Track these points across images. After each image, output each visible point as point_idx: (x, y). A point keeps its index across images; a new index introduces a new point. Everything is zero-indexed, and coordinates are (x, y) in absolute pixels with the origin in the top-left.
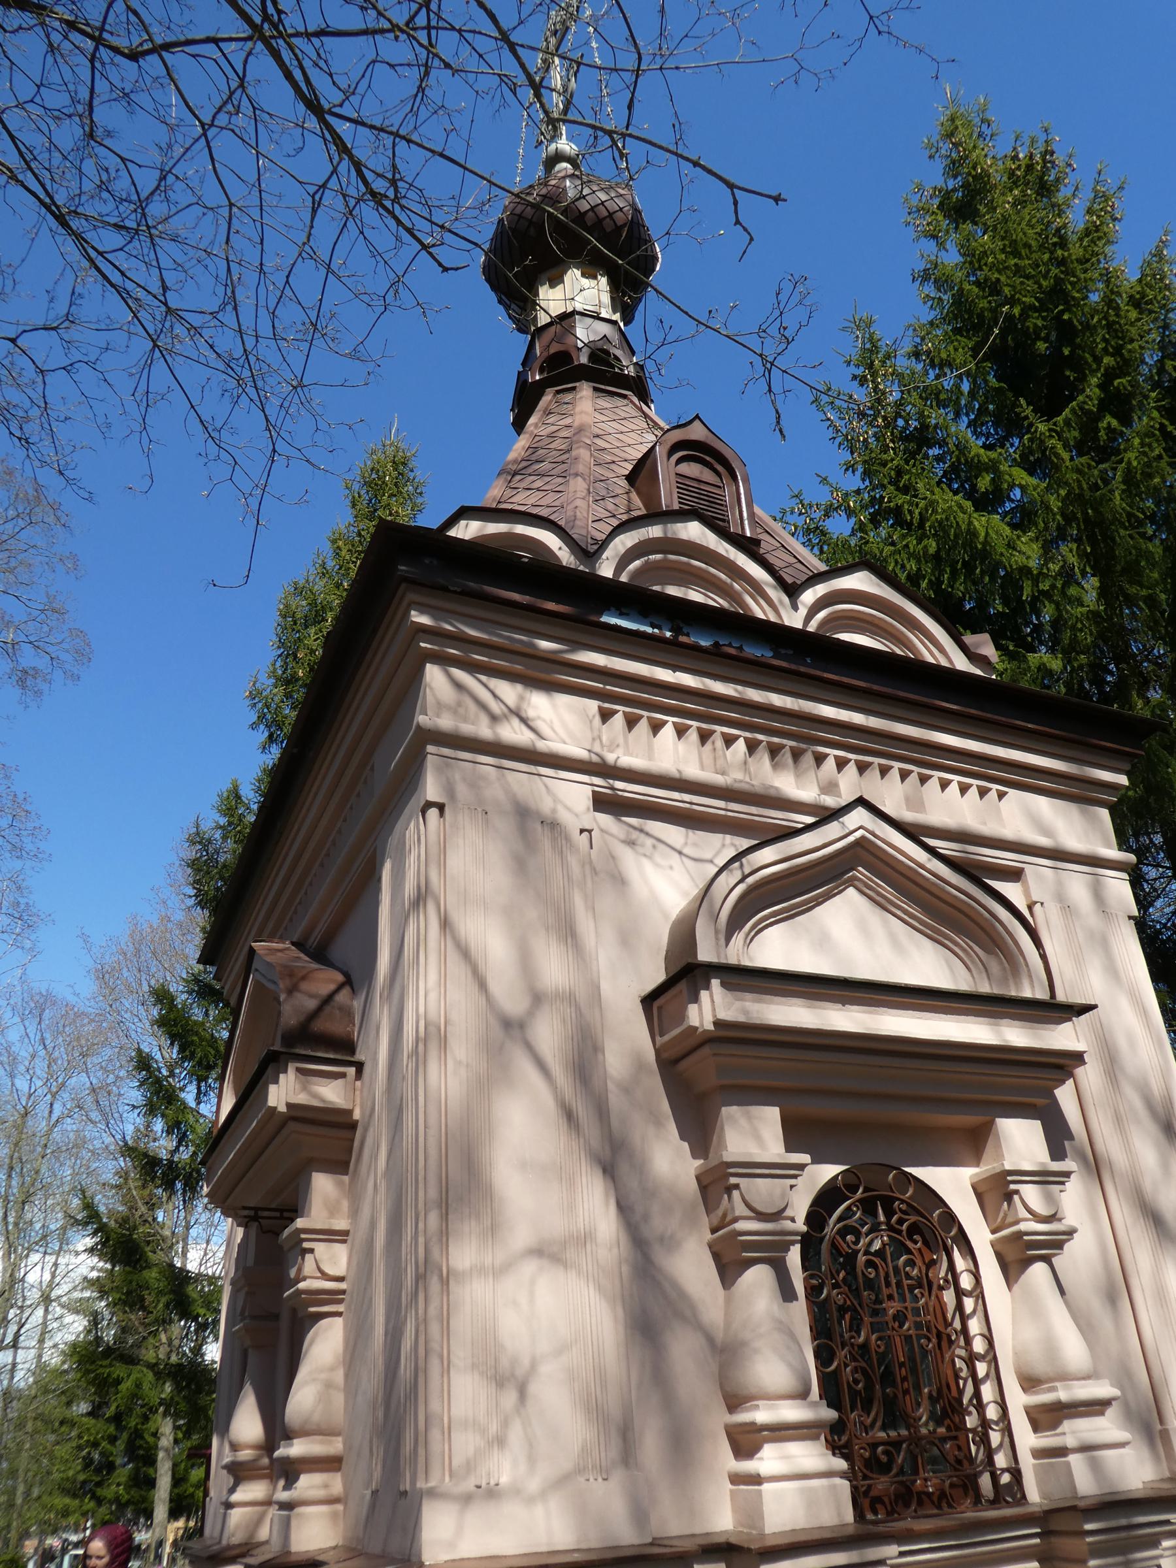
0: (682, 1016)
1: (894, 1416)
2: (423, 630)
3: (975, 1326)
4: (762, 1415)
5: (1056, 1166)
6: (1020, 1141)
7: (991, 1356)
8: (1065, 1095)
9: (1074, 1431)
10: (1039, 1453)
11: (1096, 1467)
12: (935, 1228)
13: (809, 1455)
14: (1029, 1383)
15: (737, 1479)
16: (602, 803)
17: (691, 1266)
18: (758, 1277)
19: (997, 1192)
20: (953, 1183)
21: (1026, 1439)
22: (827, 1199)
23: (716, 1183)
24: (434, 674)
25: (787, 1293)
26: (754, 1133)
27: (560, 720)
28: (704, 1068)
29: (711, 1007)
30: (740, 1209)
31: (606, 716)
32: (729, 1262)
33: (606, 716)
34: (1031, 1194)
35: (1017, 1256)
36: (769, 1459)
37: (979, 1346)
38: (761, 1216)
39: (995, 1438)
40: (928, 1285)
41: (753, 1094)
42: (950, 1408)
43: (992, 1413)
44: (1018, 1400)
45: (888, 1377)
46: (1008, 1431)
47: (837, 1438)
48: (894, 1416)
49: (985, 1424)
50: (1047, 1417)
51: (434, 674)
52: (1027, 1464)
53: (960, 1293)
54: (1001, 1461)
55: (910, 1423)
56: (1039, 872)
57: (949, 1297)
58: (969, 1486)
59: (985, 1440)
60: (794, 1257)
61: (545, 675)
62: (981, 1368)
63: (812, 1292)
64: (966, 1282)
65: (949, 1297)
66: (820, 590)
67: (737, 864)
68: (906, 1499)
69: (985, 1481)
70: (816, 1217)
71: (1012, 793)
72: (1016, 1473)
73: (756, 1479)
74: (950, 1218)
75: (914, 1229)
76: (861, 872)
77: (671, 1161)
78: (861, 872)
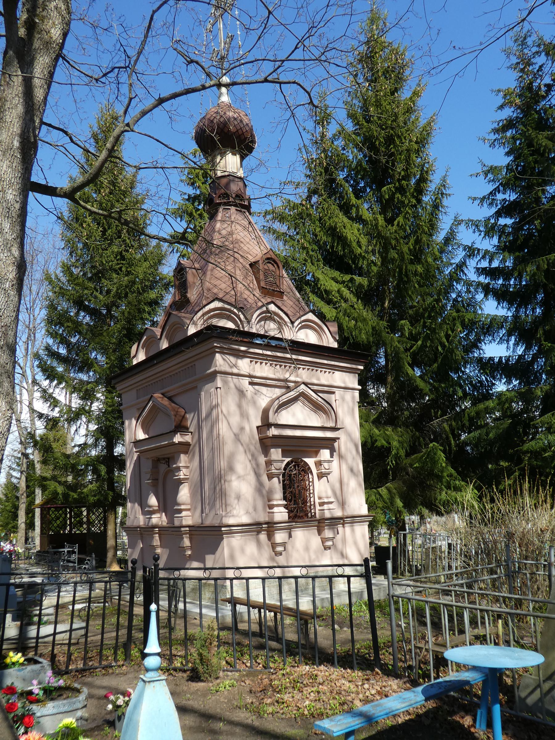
0: (266, 433)
1: (296, 503)
2: (216, 346)
3: (311, 488)
4: (275, 503)
5: (332, 459)
6: (325, 454)
7: (313, 493)
8: (336, 445)
9: (326, 507)
10: (319, 510)
11: (330, 512)
12: (306, 470)
13: (282, 509)
14: (320, 498)
15: (269, 513)
16: (251, 383)
17: (265, 478)
18: (275, 480)
19: (319, 464)
20: (310, 462)
21: (318, 507)
22: (288, 464)
23: (269, 463)
24: (218, 356)
25: (280, 482)
26: (276, 454)
27: (244, 365)
28: (268, 442)
29: (274, 431)
30: (273, 468)
31: (251, 361)
32: (270, 477)
33: (251, 361)
34: (326, 465)
35: (321, 476)
36: (276, 510)
37: (311, 491)
38: (277, 469)
39: (312, 507)
40: (303, 480)
41: (276, 446)
42: (305, 502)
43: (312, 503)
44: (317, 501)
45: (295, 497)
46: (315, 506)
47: (286, 507)
48: (296, 503)
49: (311, 505)
50: (321, 504)
51: (218, 356)
52: (317, 512)
53: (309, 482)
54: (313, 511)
55: (298, 504)
56: (338, 392)
57: (307, 483)
58: (307, 515)
59: (310, 507)
60: (281, 477)
61: (239, 355)
62: (311, 495)
63: (283, 481)
64: (311, 480)
65: (307, 483)
66: (299, 321)
67: (224, 299)
68: (296, 516)
69: (309, 514)
70: (285, 469)
71: (336, 372)
72: (315, 513)
73: (273, 513)
74: (309, 468)
75: (303, 470)
76: (301, 398)
77: (262, 459)
78: (301, 398)
